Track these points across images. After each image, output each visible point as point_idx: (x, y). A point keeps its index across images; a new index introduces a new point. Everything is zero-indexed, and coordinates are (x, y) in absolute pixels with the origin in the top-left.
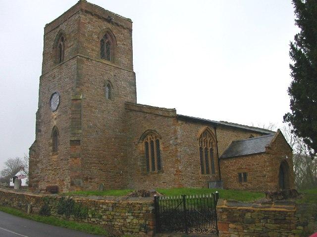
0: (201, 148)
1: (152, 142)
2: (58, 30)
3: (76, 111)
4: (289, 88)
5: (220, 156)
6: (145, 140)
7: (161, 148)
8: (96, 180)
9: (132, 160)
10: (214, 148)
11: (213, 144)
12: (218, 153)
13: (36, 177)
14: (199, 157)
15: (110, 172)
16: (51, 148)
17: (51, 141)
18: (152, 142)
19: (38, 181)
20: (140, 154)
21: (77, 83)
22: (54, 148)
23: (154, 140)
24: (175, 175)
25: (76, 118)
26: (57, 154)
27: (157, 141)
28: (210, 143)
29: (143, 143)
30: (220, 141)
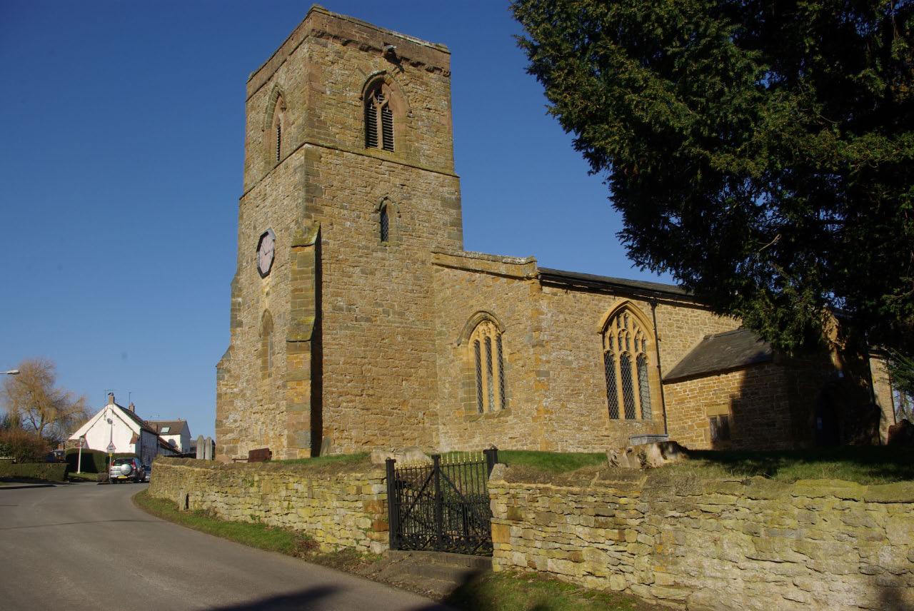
0: (608, 358)
1: (488, 341)
2: (272, 84)
3: (302, 272)
4: (611, 199)
5: (663, 376)
6: (474, 337)
7: (506, 356)
8: (353, 433)
9: (447, 385)
10: (651, 355)
11: (647, 343)
12: (659, 367)
13: (231, 431)
14: (603, 376)
15: (390, 414)
16: (259, 362)
17: (259, 346)
18: (488, 341)
19: (235, 440)
20: (462, 370)
21: (307, 208)
22: (265, 362)
23: (493, 336)
24: (534, 419)
25: (301, 290)
26: (270, 376)
27: (499, 340)
28: (636, 341)
29: (471, 345)
30: (665, 336)
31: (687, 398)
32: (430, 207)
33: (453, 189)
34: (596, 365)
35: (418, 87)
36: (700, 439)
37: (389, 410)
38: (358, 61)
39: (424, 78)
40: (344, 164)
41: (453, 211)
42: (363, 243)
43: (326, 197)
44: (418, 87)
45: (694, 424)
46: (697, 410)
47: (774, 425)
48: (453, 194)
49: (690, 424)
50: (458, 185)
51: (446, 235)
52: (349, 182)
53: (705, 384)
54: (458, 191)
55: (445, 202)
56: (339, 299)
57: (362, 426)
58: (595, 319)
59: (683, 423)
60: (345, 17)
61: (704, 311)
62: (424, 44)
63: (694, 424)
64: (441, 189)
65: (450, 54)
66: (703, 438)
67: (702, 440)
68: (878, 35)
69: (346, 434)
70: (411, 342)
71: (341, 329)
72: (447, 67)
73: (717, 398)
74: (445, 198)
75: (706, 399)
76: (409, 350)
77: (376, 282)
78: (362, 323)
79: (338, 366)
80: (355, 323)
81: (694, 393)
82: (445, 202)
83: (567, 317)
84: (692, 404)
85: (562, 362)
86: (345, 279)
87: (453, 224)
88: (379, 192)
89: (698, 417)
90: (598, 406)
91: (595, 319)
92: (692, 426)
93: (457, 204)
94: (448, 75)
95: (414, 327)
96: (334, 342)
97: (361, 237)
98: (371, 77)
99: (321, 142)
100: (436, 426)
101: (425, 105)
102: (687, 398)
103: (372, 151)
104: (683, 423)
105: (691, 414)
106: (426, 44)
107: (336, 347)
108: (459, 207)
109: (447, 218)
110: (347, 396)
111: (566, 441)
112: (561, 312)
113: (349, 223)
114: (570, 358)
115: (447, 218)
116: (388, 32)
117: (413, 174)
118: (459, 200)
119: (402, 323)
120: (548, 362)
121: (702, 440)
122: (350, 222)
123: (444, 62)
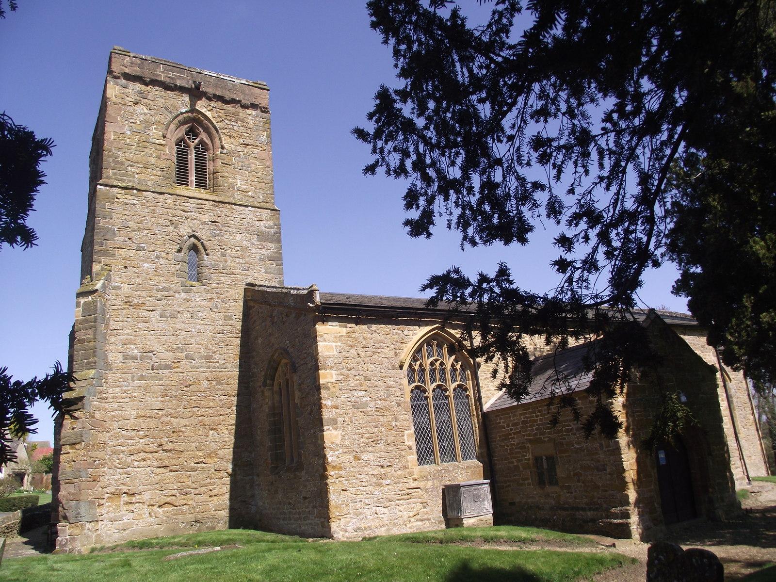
31: (510, 434)
32: (245, 242)
33: (271, 223)
34: (399, 405)
35: (233, 123)
36: (526, 482)
37: (192, 464)
38: (163, 101)
39: (241, 114)
40: (142, 204)
41: (272, 246)
42: (164, 285)
43: (119, 240)
44: (233, 123)
45: (519, 464)
46: (521, 448)
47: (605, 470)
48: (271, 227)
49: (515, 464)
50: (279, 218)
51: (263, 270)
52: (148, 222)
53: (527, 418)
54: (278, 225)
55: (262, 237)
56: (133, 346)
57: (157, 486)
58: (398, 351)
59: (509, 463)
60: (148, 58)
61: (233, 372)
62: (238, 81)
63: (519, 464)
64: (258, 223)
65: (268, 90)
66: (530, 481)
67: (529, 484)
68: (732, 326)
69: (138, 497)
70: (219, 387)
71: (133, 380)
72: (264, 103)
73: (541, 434)
74: (263, 233)
75: (529, 435)
76: (217, 396)
77: (178, 326)
78: (160, 371)
79: (128, 421)
80: (152, 372)
81: (517, 429)
82: (262, 237)
83: (361, 351)
84: (516, 441)
85: (353, 406)
86: (141, 325)
87: (271, 259)
88: (185, 230)
89: (523, 456)
90: (403, 453)
91: (398, 351)
92: (517, 467)
93: (277, 238)
94: (265, 110)
95: (224, 370)
96: (124, 395)
97: (161, 279)
98: (178, 116)
99: (115, 183)
100: (251, 477)
101: (241, 141)
102: (510, 434)
103: (181, 190)
104: (509, 463)
105: (516, 453)
106: (242, 82)
107: (126, 400)
108: (279, 241)
109: (265, 252)
110: (139, 455)
111: (361, 501)
112: (352, 347)
113: (146, 265)
114: (364, 400)
115: (265, 252)
116: (199, 71)
117: (225, 210)
118: (279, 233)
119: (208, 367)
120: (336, 407)
121: (529, 484)
122: (148, 263)
123: (263, 98)
